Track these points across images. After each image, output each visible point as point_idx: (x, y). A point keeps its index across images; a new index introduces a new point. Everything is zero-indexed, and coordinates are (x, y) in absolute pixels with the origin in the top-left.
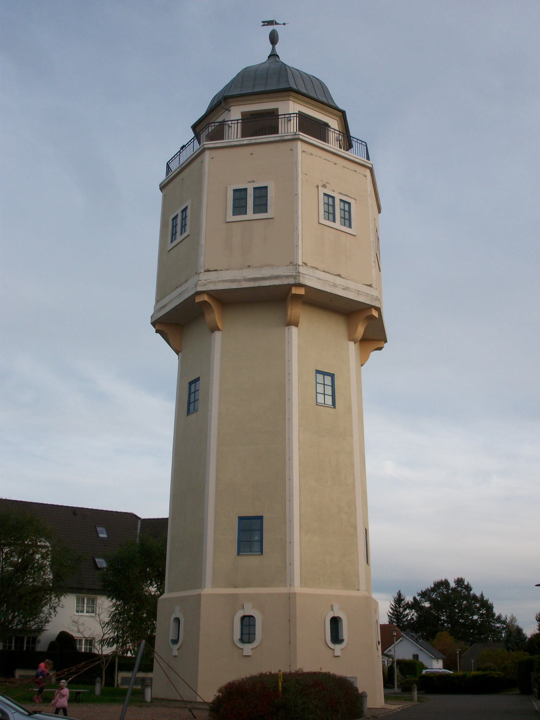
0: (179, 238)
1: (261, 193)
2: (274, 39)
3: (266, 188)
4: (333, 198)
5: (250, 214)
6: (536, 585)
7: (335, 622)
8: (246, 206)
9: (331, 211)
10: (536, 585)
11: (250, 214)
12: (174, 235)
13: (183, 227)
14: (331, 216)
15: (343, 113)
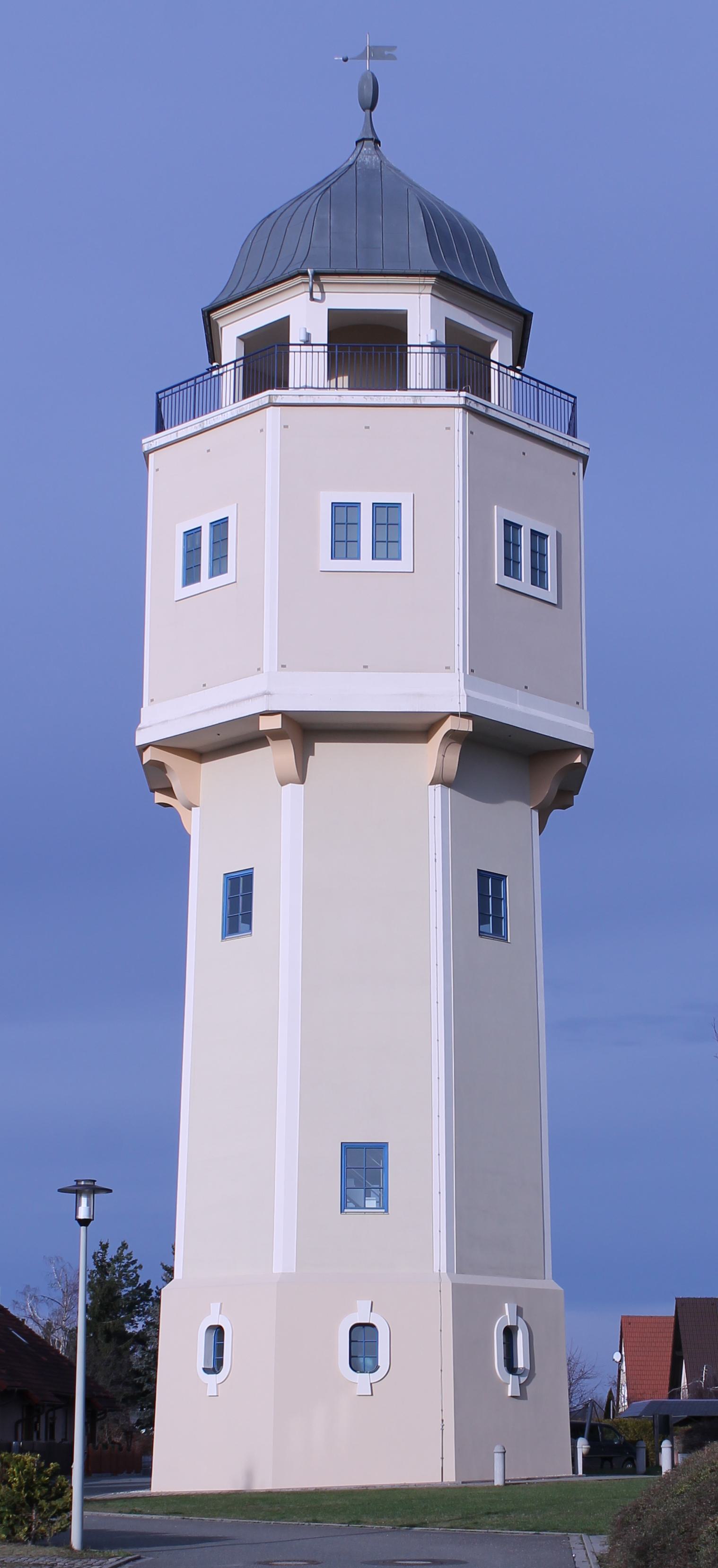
0: (206, 582)
1: (387, 515)
3: (399, 505)
5: (366, 560)
6: (60, 1190)
7: (218, 1332)
8: (357, 542)
10: (60, 1190)
11: (366, 560)
13: (219, 564)
15: (526, 317)
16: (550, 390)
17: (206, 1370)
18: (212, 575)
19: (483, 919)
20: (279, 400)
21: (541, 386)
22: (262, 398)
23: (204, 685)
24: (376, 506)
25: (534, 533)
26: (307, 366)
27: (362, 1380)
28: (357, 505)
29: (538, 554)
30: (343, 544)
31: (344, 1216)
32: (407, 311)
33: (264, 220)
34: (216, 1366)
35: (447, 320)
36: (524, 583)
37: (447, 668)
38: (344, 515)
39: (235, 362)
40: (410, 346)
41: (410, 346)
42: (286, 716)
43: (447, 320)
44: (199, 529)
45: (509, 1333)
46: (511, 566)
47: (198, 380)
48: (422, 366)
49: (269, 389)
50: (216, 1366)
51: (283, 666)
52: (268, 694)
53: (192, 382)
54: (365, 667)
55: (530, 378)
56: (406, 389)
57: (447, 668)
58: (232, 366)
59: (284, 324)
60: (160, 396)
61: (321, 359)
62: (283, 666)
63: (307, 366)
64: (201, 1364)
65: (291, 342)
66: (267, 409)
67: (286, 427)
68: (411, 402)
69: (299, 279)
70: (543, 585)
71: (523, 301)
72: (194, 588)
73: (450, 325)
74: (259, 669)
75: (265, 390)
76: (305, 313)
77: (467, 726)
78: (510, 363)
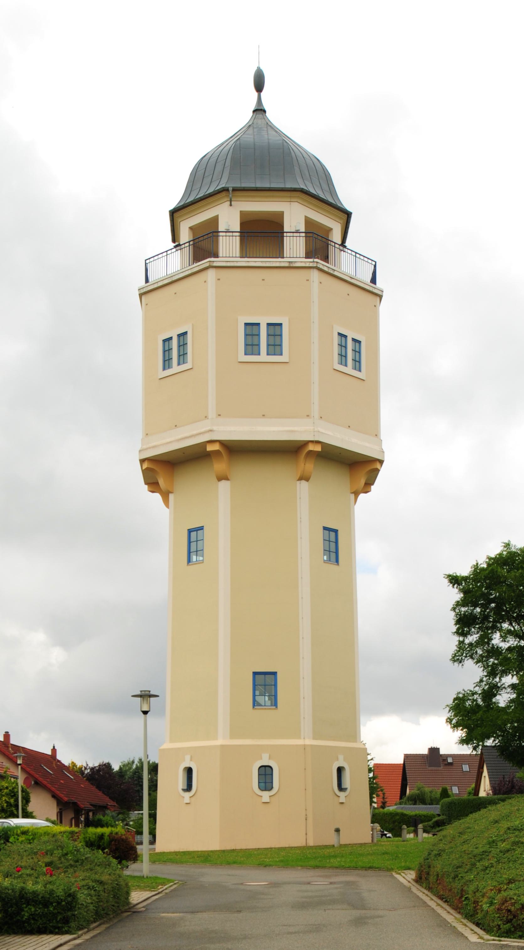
0: (175, 368)
1: (275, 329)
2: (259, 85)
3: (280, 325)
4: (346, 337)
5: (263, 356)
7: (189, 771)
9: (333, 548)
11: (263, 356)
12: (167, 363)
13: (182, 356)
14: (333, 555)
15: (348, 215)
16: (362, 257)
17: (184, 790)
18: (179, 364)
19: (327, 551)
20: (215, 264)
21: (357, 255)
22: (205, 263)
23: (176, 426)
24: (268, 324)
25: (353, 340)
26: (229, 246)
27: (266, 796)
28: (258, 324)
29: (357, 352)
30: (252, 347)
31: (256, 711)
32: (283, 212)
33: (204, 156)
34: (189, 787)
35: (306, 216)
36: (349, 369)
37: (308, 416)
38: (252, 329)
39: (189, 242)
40: (287, 232)
41: (287, 232)
42: (222, 443)
43: (306, 216)
44: (171, 338)
45: (340, 770)
46: (343, 357)
47: (169, 252)
48: (295, 247)
49: (209, 258)
50: (189, 787)
51: (219, 415)
52: (211, 431)
53: (165, 254)
54: (264, 415)
55: (352, 251)
56: (283, 258)
57: (308, 416)
58: (187, 244)
59: (215, 221)
60: (147, 261)
61: (236, 241)
62: (219, 415)
63: (229, 246)
64: (189, 335)
65: (220, 230)
66: (211, 843)
67: (219, 279)
68: (287, 265)
69: (224, 194)
70: (360, 370)
71: (347, 205)
72: (168, 372)
73: (309, 222)
74: (206, 417)
75: (206, 258)
76: (229, 216)
77: (318, 448)
78: (340, 243)
